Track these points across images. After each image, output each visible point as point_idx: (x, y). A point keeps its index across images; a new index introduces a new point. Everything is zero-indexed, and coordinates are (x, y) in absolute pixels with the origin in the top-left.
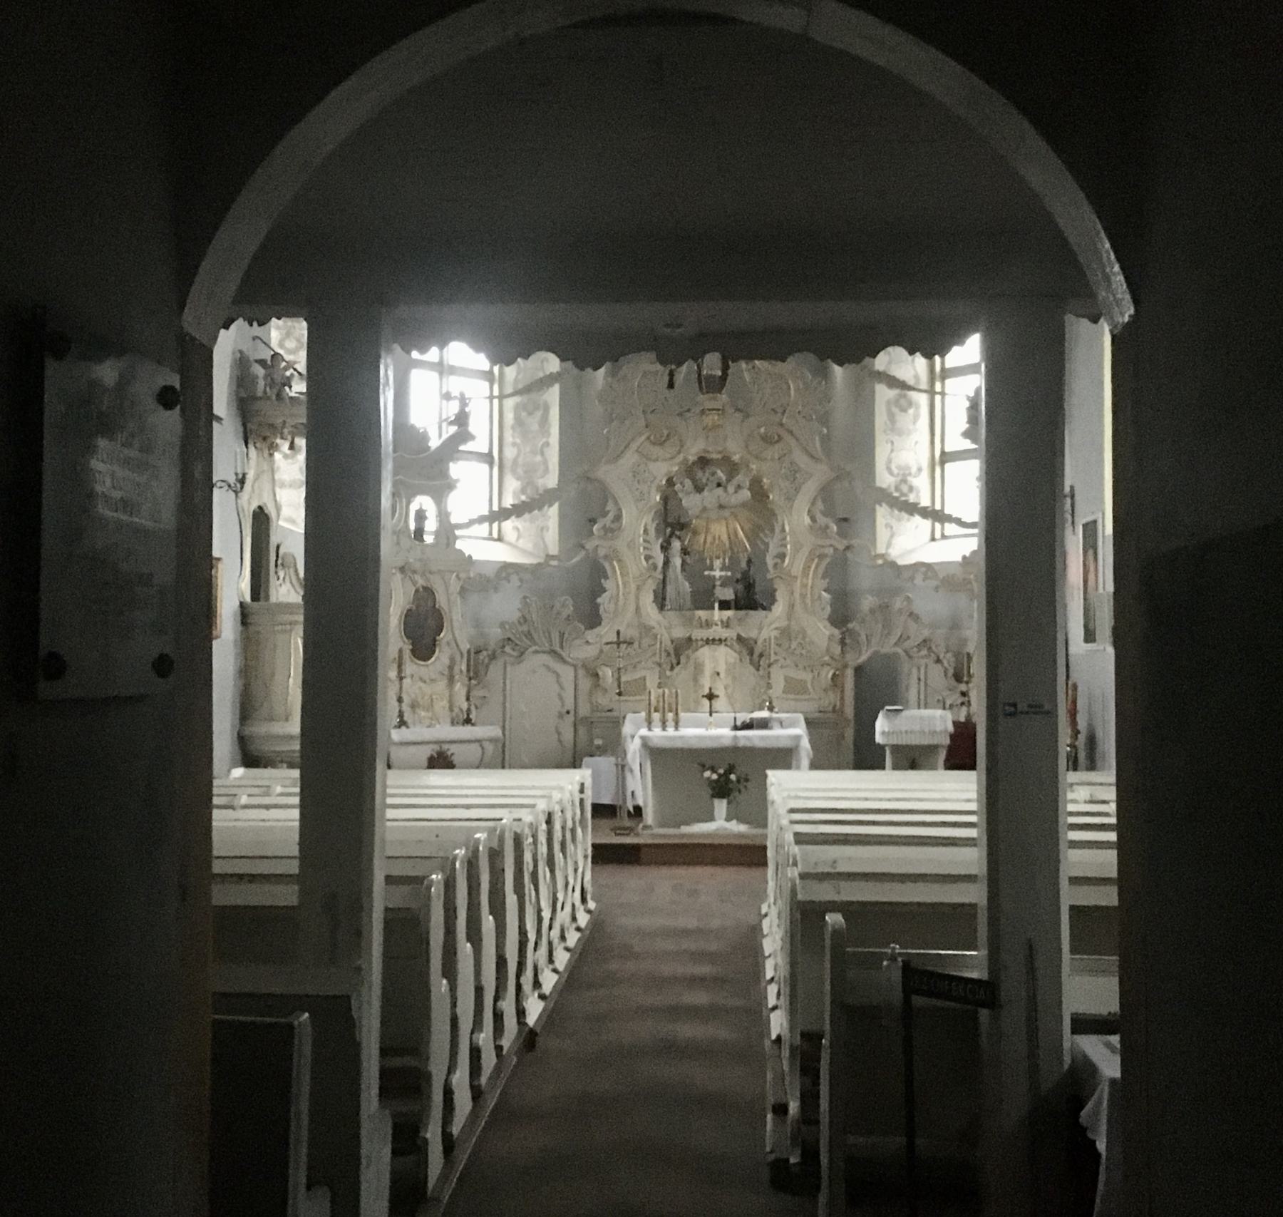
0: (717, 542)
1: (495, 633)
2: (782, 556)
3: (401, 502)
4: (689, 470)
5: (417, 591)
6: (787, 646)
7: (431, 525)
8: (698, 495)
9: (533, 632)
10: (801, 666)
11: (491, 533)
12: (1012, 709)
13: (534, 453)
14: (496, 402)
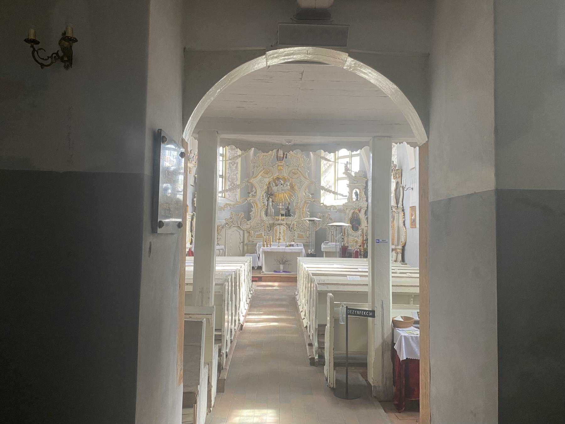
4: (274, 180)
11: (222, 196)
12: (378, 241)
14: (224, 162)
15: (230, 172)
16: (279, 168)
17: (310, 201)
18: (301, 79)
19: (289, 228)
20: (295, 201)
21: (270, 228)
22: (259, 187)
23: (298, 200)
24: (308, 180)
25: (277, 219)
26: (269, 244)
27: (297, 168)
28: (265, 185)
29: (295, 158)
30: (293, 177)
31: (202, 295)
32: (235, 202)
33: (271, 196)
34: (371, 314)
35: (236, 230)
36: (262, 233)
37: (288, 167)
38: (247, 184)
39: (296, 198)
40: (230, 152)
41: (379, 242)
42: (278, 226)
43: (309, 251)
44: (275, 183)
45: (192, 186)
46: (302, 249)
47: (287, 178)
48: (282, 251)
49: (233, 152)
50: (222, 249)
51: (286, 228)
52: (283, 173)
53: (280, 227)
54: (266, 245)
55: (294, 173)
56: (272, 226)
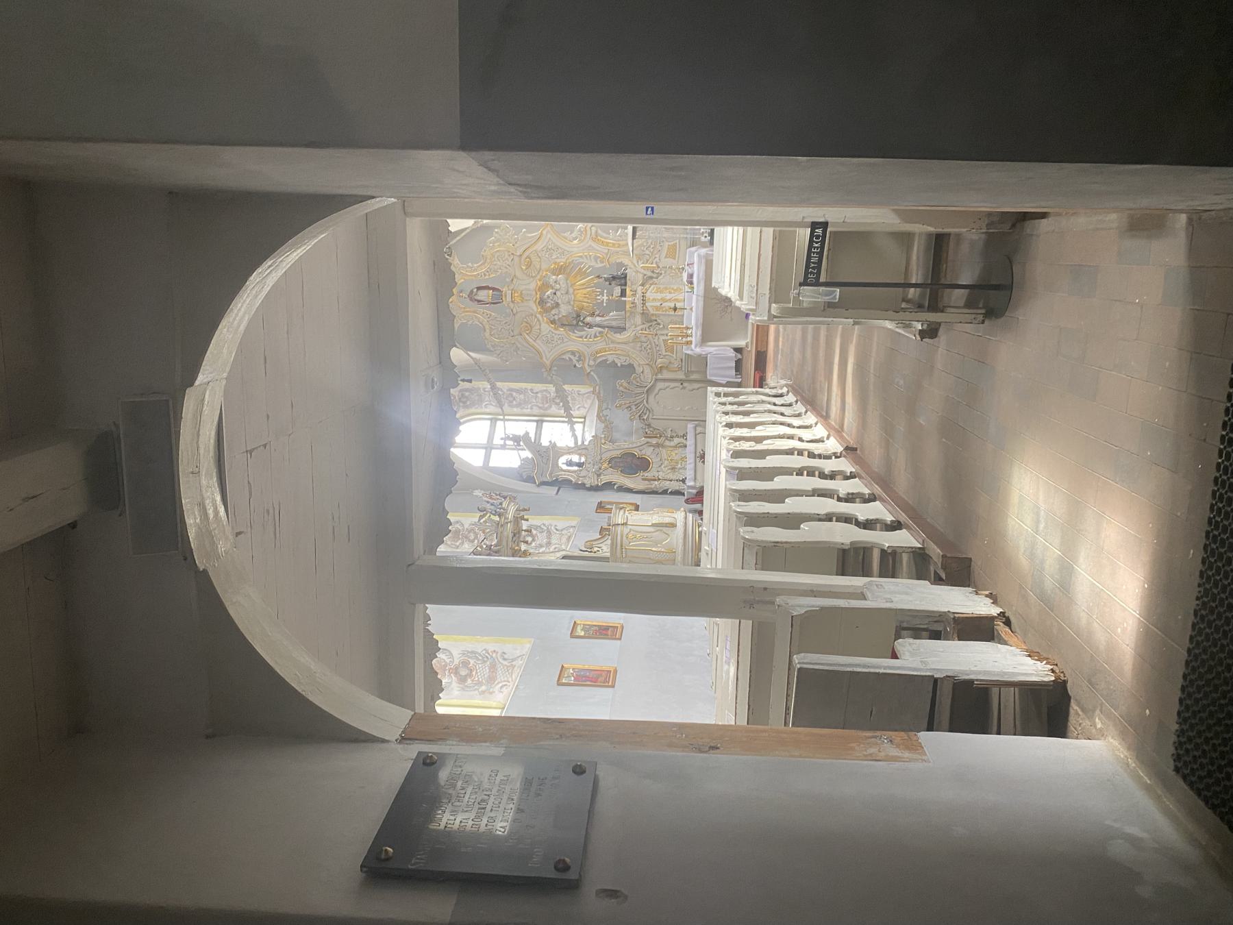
4: (546, 311)
11: (581, 422)
12: (650, 209)
14: (506, 417)
15: (529, 406)
16: (518, 300)
18: (265, 446)
19: (651, 278)
20: (593, 263)
21: (651, 321)
22: (562, 345)
26: (685, 331)
28: (556, 332)
29: (495, 263)
31: (758, 602)
33: (582, 319)
34: (819, 231)
35: (655, 397)
37: (515, 280)
38: (553, 372)
39: (585, 260)
43: (703, 239)
44: (553, 308)
45: (560, 491)
47: (540, 280)
48: (701, 304)
49: (487, 398)
50: (695, 428)
52: (529, 290)
54: (689, 339)
55: (529, 265)
56: (648, 318)
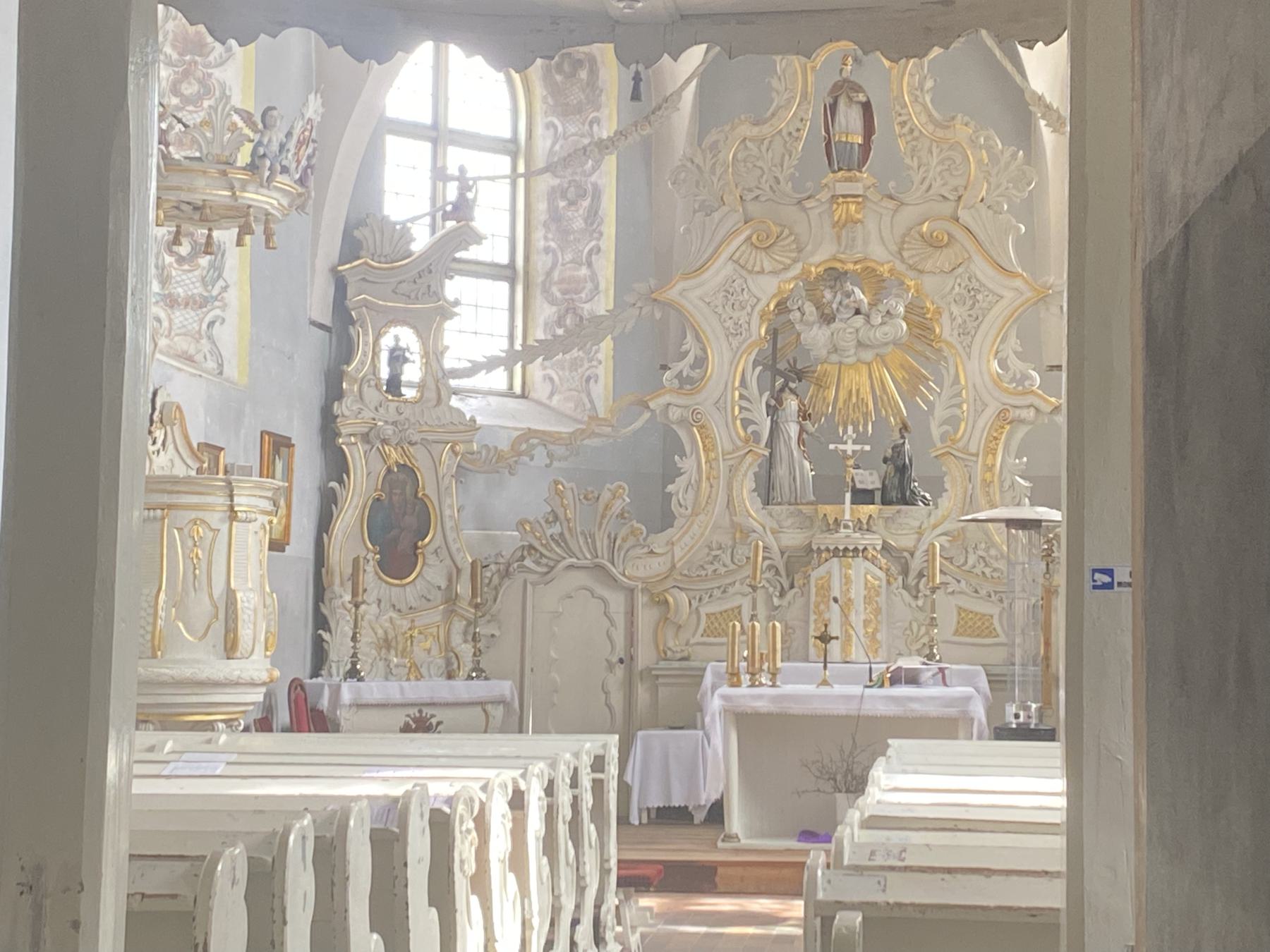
0: (854, 399)
1: (511, 538)
2: (953, 421)
3: (366, 334)
4: (811, 288)
5: (389, 471)
6: (962, 561)
7: (412, 372)
8: (824, 327)
9: (567, 536)
10: (983, 592)
11: (511, 387)
12: (1107, 579)
13: (577, 263)
14: (521, 181)
15: (553, 244)
16: (840, 213)
17: (1032, 412)
19: (905, 572)
21: (789, 574)
23: (959, 406)
24: (1018, 283)
25: (831, 522)
27: (947, 208)
30: (928, 266)
31: (38, 909)
32: (580, 422)
33: (792, 385)
36: (740, 607)
37: (891, 204)
40: (555, 128)
41: (1109, 586)
42: (835, 560)
45: (321, 332)
46: (968, 699)
48: (841, 709)
49: (572, 129)
50: (501, 701)
51: (881, 574)
52: (866, 242)
53: (849, 567)
54: (745, 678)
55: (933, 243)
56: (804, 558)
